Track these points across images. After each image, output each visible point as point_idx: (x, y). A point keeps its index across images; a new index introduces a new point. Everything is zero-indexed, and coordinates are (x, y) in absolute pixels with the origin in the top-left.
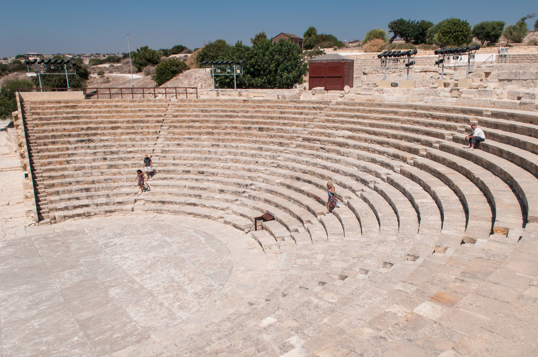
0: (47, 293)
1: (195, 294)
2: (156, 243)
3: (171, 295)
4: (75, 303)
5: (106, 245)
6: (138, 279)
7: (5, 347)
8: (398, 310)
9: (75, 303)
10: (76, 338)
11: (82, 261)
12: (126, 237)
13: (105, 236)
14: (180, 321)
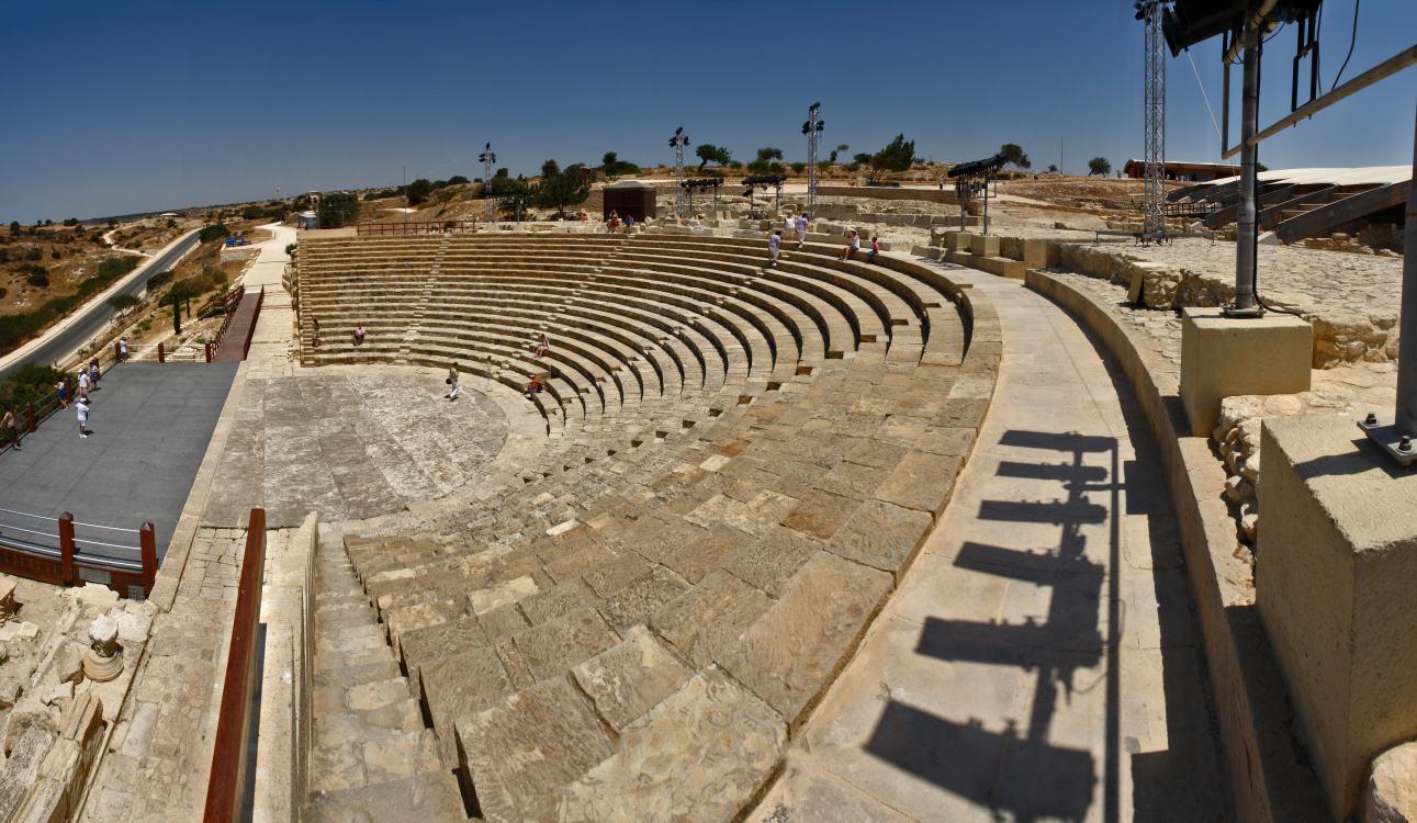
0: (307, 439)
1: (461, 464)
2: (419, 399)
3: (433, 463)
4: (332, 455)
5: (367, 396)
6: (397, 439)
7: (266, 485)
8: (684, 468)
9: (332, 455)
10: (330, 494)
11: (342, 410)
12: (387, 389)
13: (366, 385)
14: (441, 494)
